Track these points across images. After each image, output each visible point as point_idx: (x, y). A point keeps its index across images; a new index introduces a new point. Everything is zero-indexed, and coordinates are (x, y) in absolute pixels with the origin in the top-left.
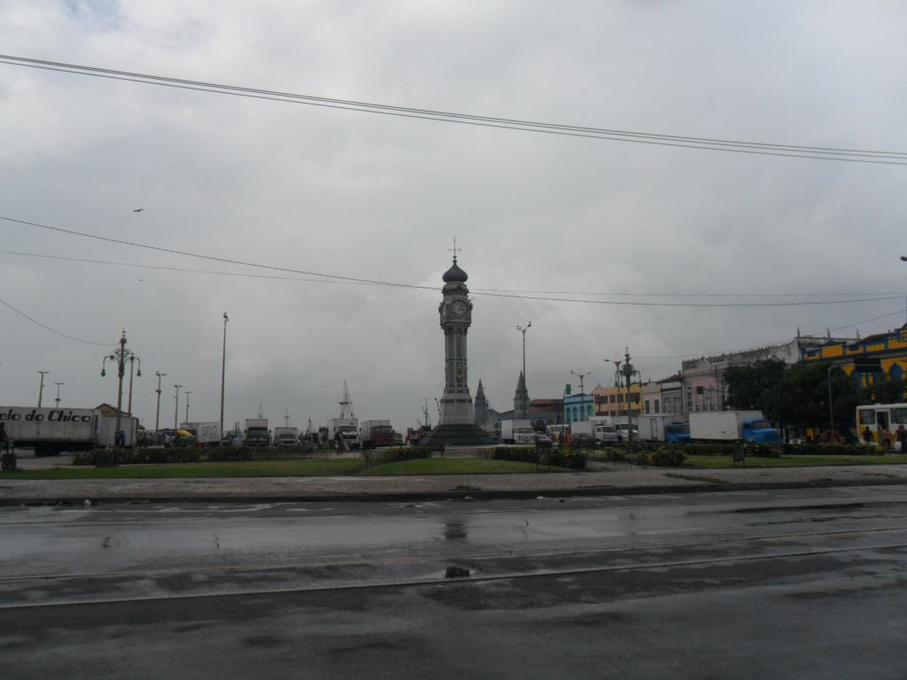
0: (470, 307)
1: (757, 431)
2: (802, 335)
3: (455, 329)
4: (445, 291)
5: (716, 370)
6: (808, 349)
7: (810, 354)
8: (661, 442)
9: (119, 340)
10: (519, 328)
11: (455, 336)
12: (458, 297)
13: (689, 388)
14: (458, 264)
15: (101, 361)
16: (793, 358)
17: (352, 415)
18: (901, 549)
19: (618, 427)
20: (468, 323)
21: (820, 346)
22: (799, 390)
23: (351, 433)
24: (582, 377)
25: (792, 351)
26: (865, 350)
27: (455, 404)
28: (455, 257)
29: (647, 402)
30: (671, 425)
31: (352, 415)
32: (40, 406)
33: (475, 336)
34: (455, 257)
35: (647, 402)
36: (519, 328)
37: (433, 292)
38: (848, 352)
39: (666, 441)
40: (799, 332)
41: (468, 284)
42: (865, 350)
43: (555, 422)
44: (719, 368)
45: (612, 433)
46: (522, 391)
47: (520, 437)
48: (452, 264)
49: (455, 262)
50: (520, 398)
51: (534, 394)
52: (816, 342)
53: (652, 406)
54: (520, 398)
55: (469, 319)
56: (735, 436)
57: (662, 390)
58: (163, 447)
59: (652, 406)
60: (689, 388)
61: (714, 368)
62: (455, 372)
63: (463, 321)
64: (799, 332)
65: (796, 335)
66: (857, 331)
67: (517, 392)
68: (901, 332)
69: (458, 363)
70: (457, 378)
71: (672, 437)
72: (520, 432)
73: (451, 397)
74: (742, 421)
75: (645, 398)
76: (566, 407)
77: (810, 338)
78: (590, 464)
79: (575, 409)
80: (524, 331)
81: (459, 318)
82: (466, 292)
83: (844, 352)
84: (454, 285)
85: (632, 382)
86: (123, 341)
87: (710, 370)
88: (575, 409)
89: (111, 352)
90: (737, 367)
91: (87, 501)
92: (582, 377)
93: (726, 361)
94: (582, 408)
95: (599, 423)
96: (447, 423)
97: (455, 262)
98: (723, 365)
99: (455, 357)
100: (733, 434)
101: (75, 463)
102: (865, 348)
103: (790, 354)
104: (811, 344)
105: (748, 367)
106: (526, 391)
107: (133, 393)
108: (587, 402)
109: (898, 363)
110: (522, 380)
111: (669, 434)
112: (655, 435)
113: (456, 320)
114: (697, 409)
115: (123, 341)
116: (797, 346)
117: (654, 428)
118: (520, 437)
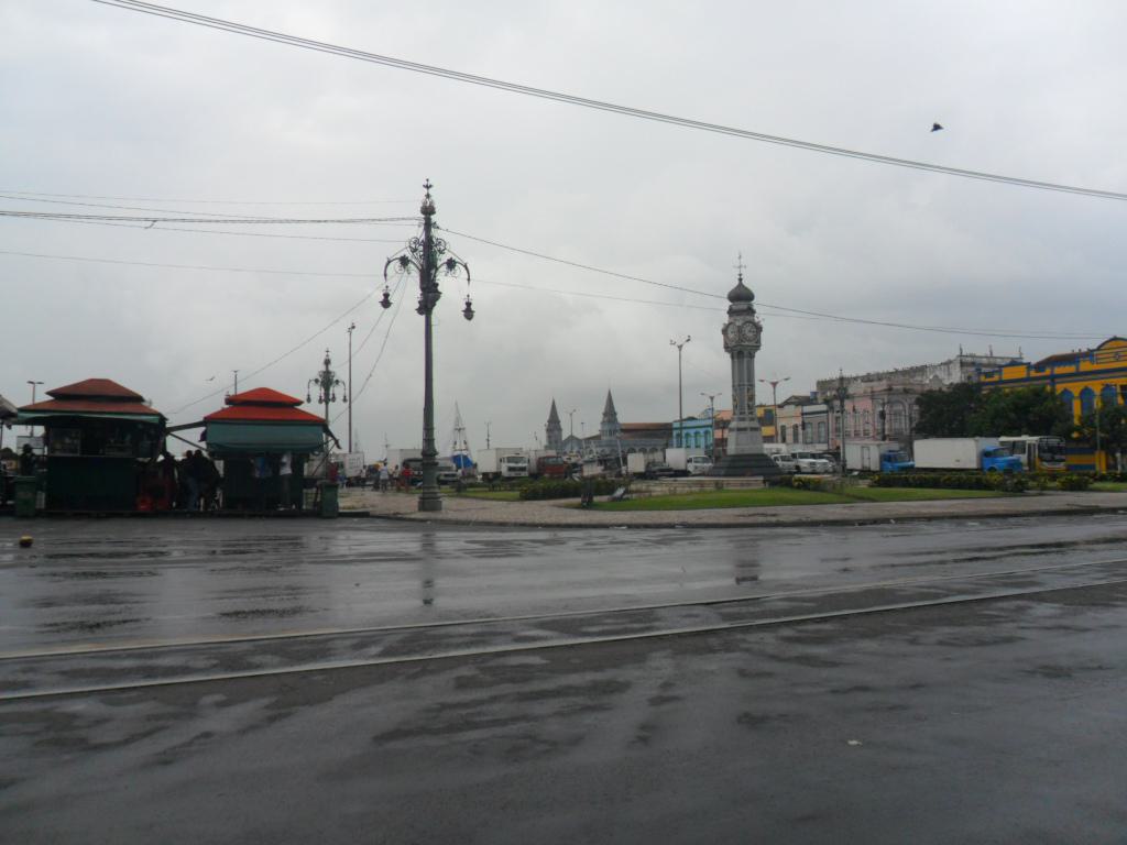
0: (759, 329)
1: (999, 459)
2: (964, 354)
3: (746, 353)
4: (731, 312)
5: (872, 392)
6: (984, 370)
7: (987, 375)
8: (874, 472)
9: (322, 361)
10: (673, 343)
11: (745, 360)
12: (748, 318)
15: (306, 385)
16: (956, 376)
17: (465, 443)
18: (446, 641)
19: (794, 456)
20: (758, 347)
21: (1001, 366)
22: (1012, 415)
23: (520, 465)
24: (712, 398)
25: (952, 371)
26: (1052, 372)
29: (783, 428)
30: (888, 453)
31: (465, 443)
33: (762, 362)
35: (783, 428)
36: (673, 343)
37: (720, 312)
38: (1033, 374)
39: (881, 470)
40: (961, 350)
41: (756, 304)
42: (1052, 372)
44: (875, 389)
45: (790, 463)
46: (610, 413)
47: (696, 468)
48: (737, 283)
49: (740, 280)
50: (609, 421)
51: (626, 417)
52: (978, 360)
53: (789, 432)
54: (609, 421)
55: (759, 341)
56: (973, 465)
57: (803, 414)
58: (622, 479)
59: (789, 432)
61: (869, 390)
62: (746, 398)
63: (753, 343)
64: (961, 350)
65: (958, 353)
66: (990, 346)
67: (605, 414)
71: (889, 466)
72: (509, 462)
74: (981, 449)
75: (780, 423)
76: (675, 433)
77: (972, 356)
78: (347, 500)
79: (687, 435)
80: (680, 347)
81: (749, 341)
82: (753, 312)
83: (1028, 373)
84: (742, 306)
86: (327, 362)
87: (865, 392)
88: (687, 435)
89: (316, 375)
90: (931, 391)
91: (892, 521)
92: (712, 398)
93: (884, 382)
94: (696, 433)
95: (774, 451)
97: (740, 280)
98: (881, 386)
99: (746, 383)
100: (970, 461)
101: (871, 486)
102: (1052, 369)
103: (949, 374)
104: (988, 365)
105: (940, 390)
106: (615, 414)
108: (685, 428)
109: (1090, 387)
110: (554, 403)
111: (886, 463)
112: (866, 464)
113: (747, 343)
114: (865, 434)
115: (327, 362)
116: (959, 365)
117: (866, 456)
118: (696, 468)
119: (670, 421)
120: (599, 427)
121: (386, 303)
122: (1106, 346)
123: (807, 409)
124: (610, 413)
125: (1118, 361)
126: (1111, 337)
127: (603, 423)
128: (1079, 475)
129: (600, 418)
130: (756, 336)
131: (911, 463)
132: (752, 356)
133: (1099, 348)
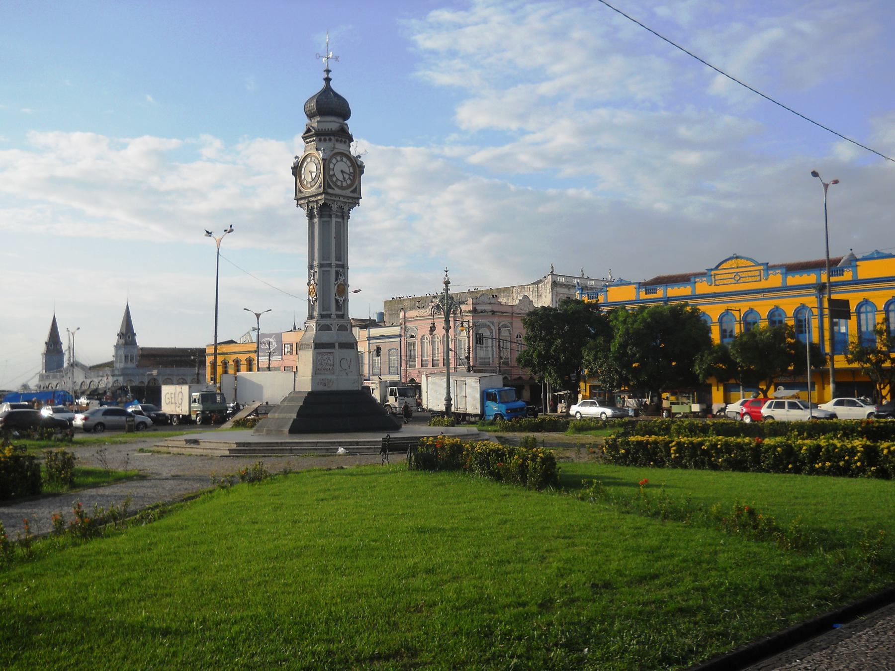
0: (357, 168)
3: (335, 207)
11: (334, 220)
12: (341, 147)
13: (412, 336)
14: (334, 86)
24: (258, 316)
27: (337, 351)
28: (328, 71)
32: (828, 258)
34: (328, 71)
41: (352, 125)
43: (845, 401)
46: (127, 334)
48: (321, 85)
49: (328, 80)
50: (126, 344)
51: (145, 340)
60: (412, 336)
62: (334, 289)
63: (347, 193)
67: (121, 335)
68: (713, 273)
69: (337, 273)
70: (337, 301)
73: (327, 337)
81: (341, 188)
83: (785, 280)
84: (332, 124)
85: (869, 314)
92: (258, 316)
96: (321, 388)
97: (328, 80)
99: (334, 262)
103: (539, 296)
106: (134, 335)
107: (824, 222)
119: (203, 346)
120: (112, 351)
121: (78, 329)
122: (724, 266)
123: (375, 332)
124: (127, 334)
125: (738, 282)
126: (731, 255)
127: (117, 347)
128: (123, 413)
129: (114, 340)
130: (353, 182)
131: (580, 401)
132: (344, 216)
133: (717, 268)
